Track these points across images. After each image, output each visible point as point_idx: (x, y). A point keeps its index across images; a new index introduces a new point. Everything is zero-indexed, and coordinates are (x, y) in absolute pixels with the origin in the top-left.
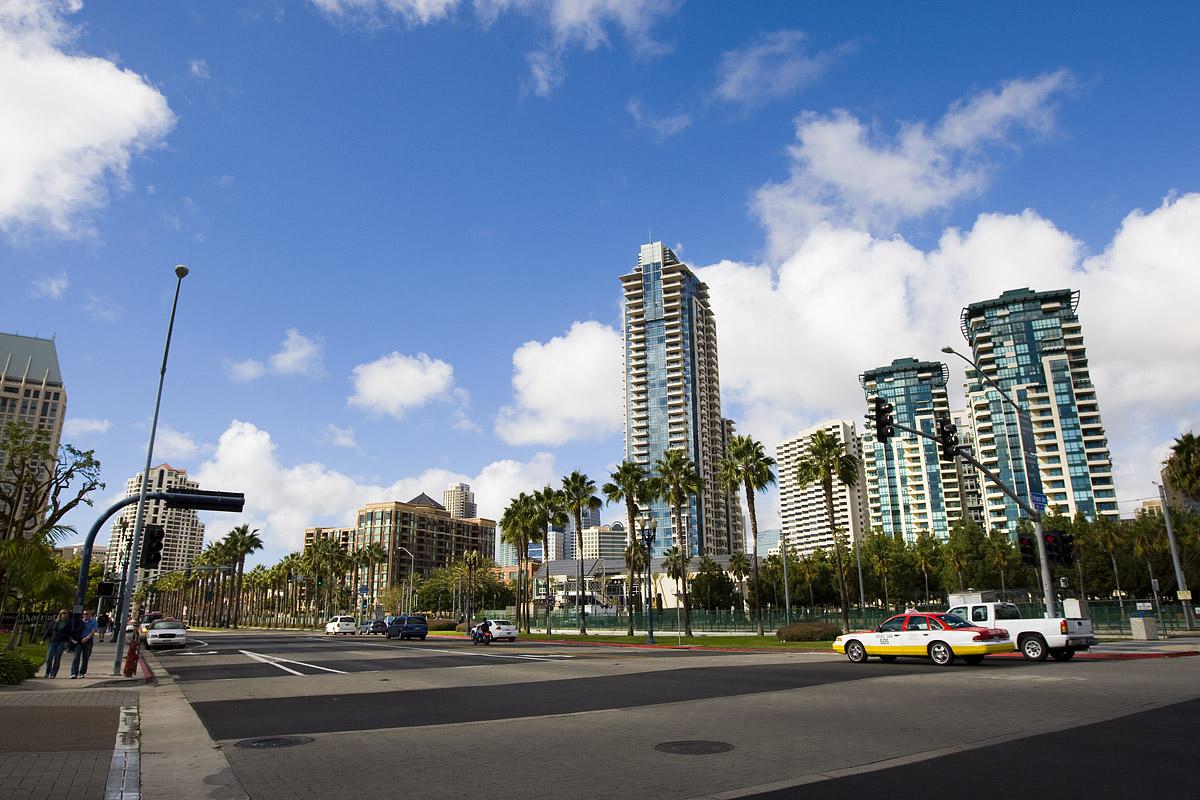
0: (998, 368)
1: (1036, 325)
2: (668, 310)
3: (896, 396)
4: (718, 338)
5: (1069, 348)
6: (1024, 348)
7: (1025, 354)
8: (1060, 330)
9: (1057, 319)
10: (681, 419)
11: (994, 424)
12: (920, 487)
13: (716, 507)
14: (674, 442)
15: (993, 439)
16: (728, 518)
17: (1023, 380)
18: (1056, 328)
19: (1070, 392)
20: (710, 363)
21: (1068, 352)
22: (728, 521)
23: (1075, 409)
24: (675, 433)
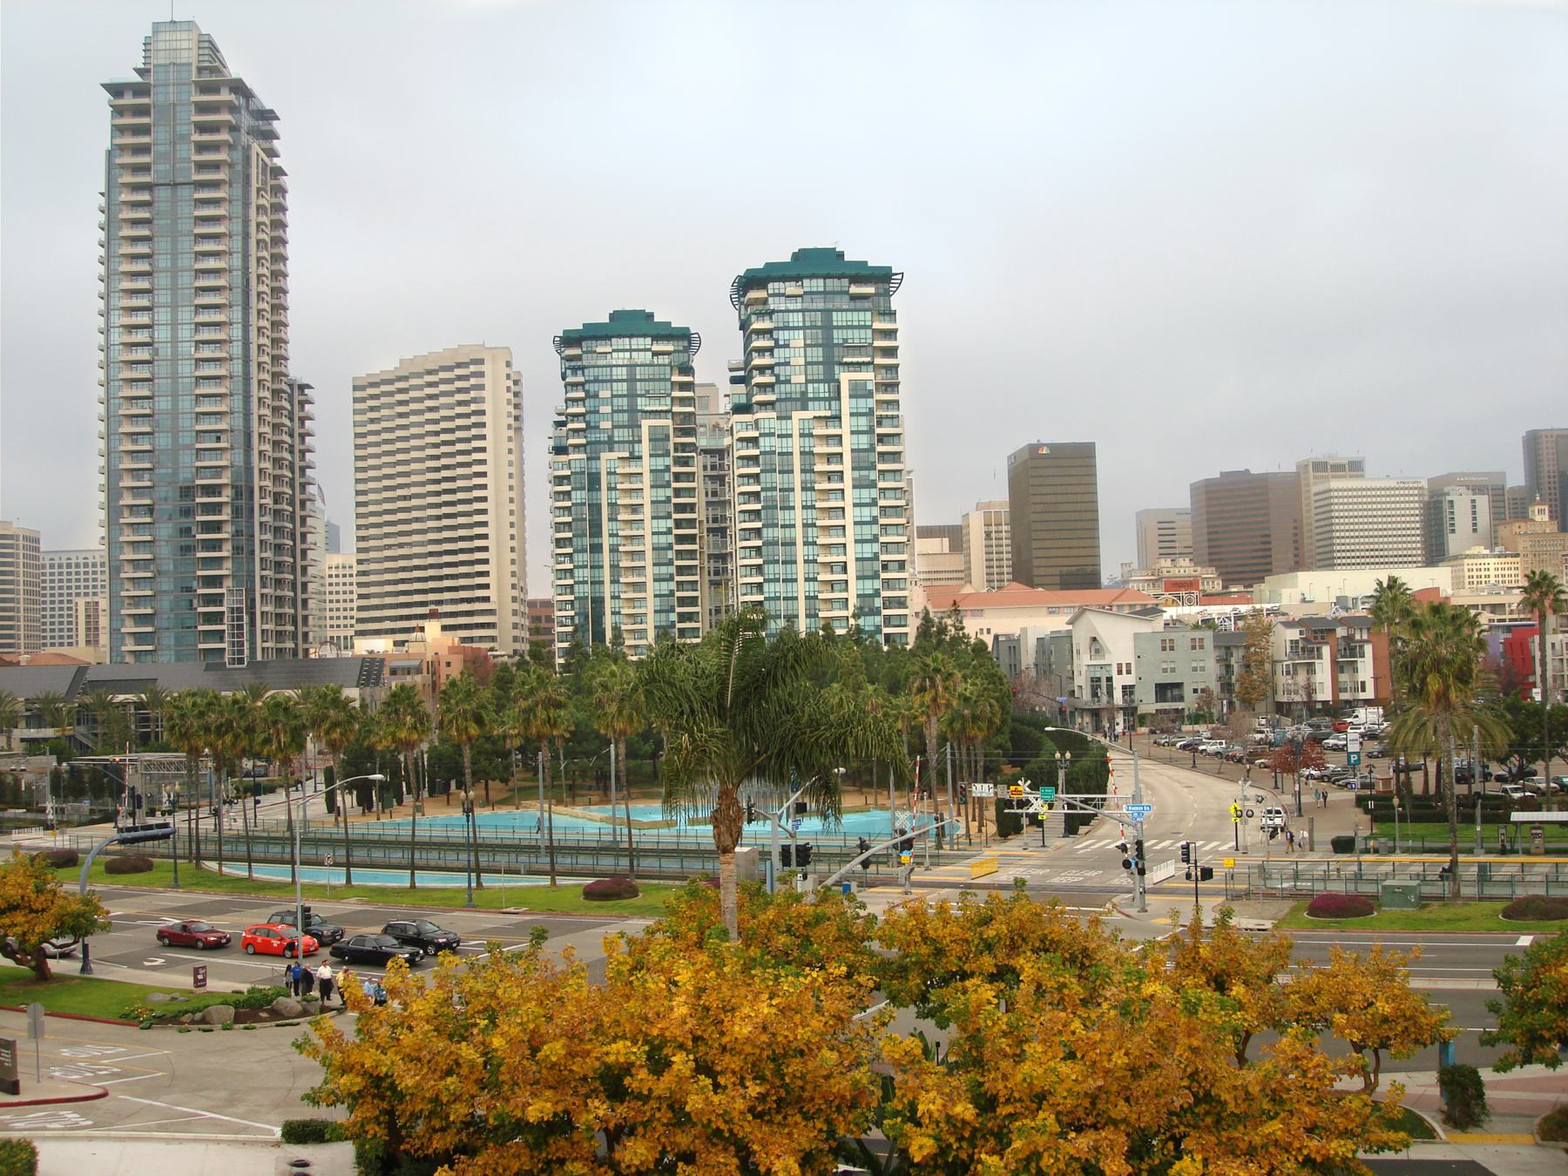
1: (838, 318)
2: (201, 166)
3: (612, 381)
5: (878, 361)
9: (869, 314)
12: (639, 587)
13: (276, 502)
15: (756, 457)
17: (810, 404)
18: (865, 327)
21: (877, 368)
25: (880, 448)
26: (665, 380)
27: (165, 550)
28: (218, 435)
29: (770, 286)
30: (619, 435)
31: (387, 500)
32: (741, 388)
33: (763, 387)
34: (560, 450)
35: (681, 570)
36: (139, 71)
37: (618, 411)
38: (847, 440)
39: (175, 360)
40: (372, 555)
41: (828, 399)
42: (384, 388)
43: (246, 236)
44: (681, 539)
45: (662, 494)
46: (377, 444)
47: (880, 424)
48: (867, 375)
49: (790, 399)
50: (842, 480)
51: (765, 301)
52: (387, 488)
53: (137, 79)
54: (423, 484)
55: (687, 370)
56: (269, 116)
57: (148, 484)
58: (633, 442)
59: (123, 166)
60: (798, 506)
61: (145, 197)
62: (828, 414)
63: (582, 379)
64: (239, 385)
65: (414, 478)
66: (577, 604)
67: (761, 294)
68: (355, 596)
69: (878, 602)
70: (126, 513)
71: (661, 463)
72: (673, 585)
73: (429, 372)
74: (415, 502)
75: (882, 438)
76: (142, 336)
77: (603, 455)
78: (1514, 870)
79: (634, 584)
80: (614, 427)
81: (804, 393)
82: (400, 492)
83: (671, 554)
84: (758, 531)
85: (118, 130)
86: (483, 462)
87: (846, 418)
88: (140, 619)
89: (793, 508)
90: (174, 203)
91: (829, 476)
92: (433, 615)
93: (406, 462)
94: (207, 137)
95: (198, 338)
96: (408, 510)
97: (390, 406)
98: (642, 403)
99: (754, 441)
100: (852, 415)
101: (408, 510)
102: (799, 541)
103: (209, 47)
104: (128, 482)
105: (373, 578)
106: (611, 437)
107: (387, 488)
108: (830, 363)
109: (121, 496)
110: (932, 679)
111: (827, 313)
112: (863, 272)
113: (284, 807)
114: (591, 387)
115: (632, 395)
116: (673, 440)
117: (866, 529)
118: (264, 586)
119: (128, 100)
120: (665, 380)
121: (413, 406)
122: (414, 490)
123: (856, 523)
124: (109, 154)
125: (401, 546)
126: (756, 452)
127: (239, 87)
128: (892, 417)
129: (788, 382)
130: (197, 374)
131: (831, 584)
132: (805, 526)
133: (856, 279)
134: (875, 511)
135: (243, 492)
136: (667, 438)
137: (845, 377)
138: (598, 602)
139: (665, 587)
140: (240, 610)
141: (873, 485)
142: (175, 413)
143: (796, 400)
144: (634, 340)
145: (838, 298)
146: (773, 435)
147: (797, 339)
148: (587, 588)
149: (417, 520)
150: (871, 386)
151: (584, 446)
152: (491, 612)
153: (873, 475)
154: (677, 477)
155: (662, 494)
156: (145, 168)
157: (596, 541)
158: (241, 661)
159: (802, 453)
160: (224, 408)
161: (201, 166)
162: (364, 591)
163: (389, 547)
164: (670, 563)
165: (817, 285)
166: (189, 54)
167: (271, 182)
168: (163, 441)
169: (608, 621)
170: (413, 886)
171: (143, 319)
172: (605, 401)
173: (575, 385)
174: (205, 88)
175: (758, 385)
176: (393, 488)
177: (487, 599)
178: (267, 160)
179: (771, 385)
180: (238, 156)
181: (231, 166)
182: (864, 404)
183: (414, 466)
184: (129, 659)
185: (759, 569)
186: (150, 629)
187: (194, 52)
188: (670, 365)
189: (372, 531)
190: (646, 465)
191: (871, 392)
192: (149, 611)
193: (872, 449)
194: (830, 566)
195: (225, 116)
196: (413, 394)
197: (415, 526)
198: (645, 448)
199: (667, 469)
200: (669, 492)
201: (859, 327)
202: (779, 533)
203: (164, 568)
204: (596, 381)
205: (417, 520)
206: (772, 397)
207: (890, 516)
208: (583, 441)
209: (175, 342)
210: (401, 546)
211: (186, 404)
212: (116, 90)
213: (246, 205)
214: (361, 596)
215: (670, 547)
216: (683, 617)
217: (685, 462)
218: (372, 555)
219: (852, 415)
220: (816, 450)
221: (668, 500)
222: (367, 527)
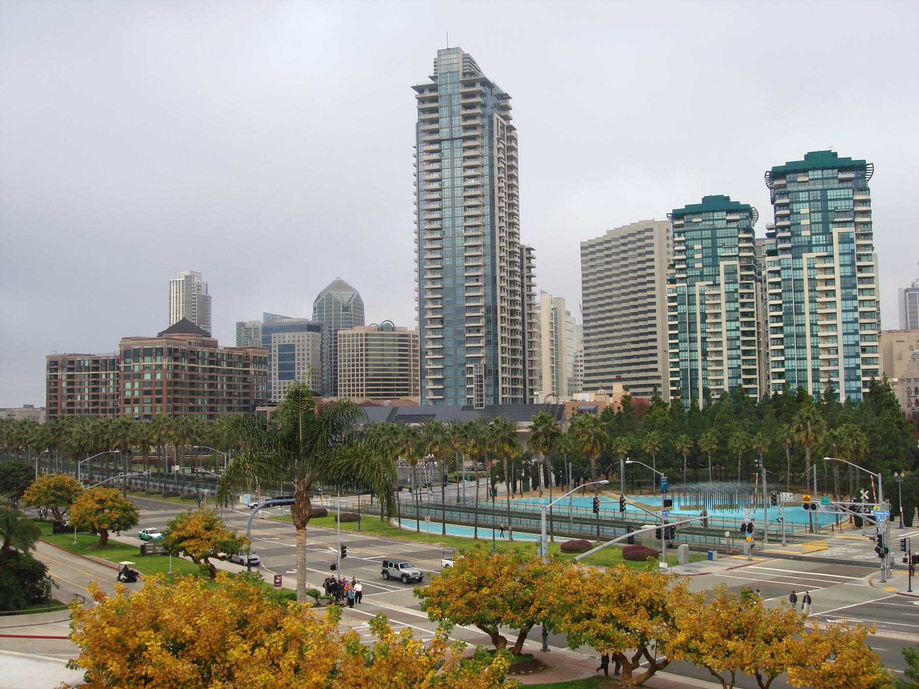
0: (792, 213)
1: (831, 194)
2: (466, 128)
4: (521, 195)
5: (858, 220)
6: (818, 217)
7: (818, 212)
8: (851, 202)
9: (851, 191)
10: (477, 192)
11: (782, 269)
13: (512, 315)
14: (470, 237)
16: (523, 298)
17: (814, 248)
18: (848, 199)
19: (852, 264)
20: (512, 206)
22: (523, 329)
23: (859, 372)
24: (470, 177)
25: (859, 275)
26: (735, 237)
27: (449, 343)
28: (477, 278)
29: (788, 177)
30: (706, 271)
31: (600, 312)
32: (773, 241)
33: (784, 239)
34: (673, 281)
35: (745, 353)
36: (430, 77)
37: (706, 257)
38: (838, 270)
39: (454, 237)
40: (592, 344)
41: (826, 245)
42: (598, 248)
43: (492, 166)
44: (744, 333)
45: (733, 306)
46: (618, 282)
47: (859, 259)
48: (850, 229)
49: (801, 246)
50: (834, 295)
51: (785, 186)
52: (600, 306)
53: (431, 82)
54: (620, 303)
55: (749, 230)
56: (506, 97)
57: (440, 306)
58: (715, 275)
59: (424, 131)
60: (807, 312)
61: (436, 147)
62: (825, 254)
63: (683, 238)
64: (488, 250)
65: (615, 299)
66: (681, 373)
67: (783, 182)
68: (583, 368)
69: (859, 372)
70: (429, 322)
71: (732, 287)
72: (740, 362)
73: (623, 237)
74: (615, 313)
75: (860, 269)
76: (436, 225)
77: (697, 284)
78: (334, 551)
79: (716, 361)
80: (704, 266)
81: (810, 242)
82: (607, 308)
83: (738, 343)
84: (781, 328)
85: (422, 111)
86: (653, 289)
87: (836, 257)
88: (436, 381)
89: (804, 314)
90: (452, 149)
91: (827, 293)
92: (619, 379)
93: (610, 290)
94: (469, 112)
95: (466, 224)
96: (611, 318)
97: (601, 258)
98: (720, 252)
99: (777, 273)
100: (840, 254)
101: (611, 318)
102: (808, 334)
103: (468, 60)
104: (430, 305)
105: (592, 357)
106: (702, 273)
107: (600, 306)
108: (826, 223)
109: (426, 313)
110: (805, 424)
111: (824, 191)
112: (847, 165)
113: (475, 489)
114: (689, 243)
115: (714, 247)
116: (740, 273)
117: (850, 326)
118: (503, 363)
119: (427, 94)
120: (735, 237)
121: (614, 258)
122: (615, 306)
123: (843, 323)
124: (418, 125)
125: (608, 338)
126: (779, 279)
127: (485, 83)
128: (868, 255)
129: (800, 235)
130: (466, 244)
131: (828, 361)
132: (812, 325)
133: (842, 169)
134: (856, 315)
135: (491, 310)
136: (736, 272)
137: (836, 231)
138: (694, 371)
139: (735, 363)
140: (481, 376)
141: (855, 298)
142: (454, 267)
143: (805, 246)
144: (716, 214)
145: (831, 181)
146: (790, 268)
147: (805, 210)
148: (688, 363)
149: (616, 323)
150: (853, 236)
151: (685, 278)
152: (659, 377)
153: (855, 292)
154: (742, 296)
155: (733, 306)
156: (436, 131)
157: (693, 335)
158: (482, 405)
159: (809, 279)
160: (480, 263)
161: (466, 128)
162: (588, 365)
163: (602, 339)
164: (738, 348)
165: (818, 174)
166: (458, 66)
167: (506, 134)
168: (448, 282)
169: (700, 384)
170: (476, 537)
171: (436, 215)
172: (698, 251)
173: (680, 242)
174: (467, 84)
175: (779, 238)
176: (603, 305)
177: (656, 370)
178: (505, 123)
179: (788, 238)
180: (486, 121)
181: (483, 127)
182: (847, 247)
183: (615, 292)
184: (430, 403)
185: (782, 352)
186: (441, 387)
187: (461, 64)
188: (738, 228)
189: (592, 331)
190: (723, 288)
191: (852, 239)
192: (441, 377)
193: (854, 275)
194: (828, 350)
195: (478, 99)
196: (613, 250)
197: (616, 327)
198: (722, 279)
199: (736, 291)
200: (737, 305)
201: (845, 199)
202: (793, 329)
203: (448, 353)
204: (692, 239)
205: (616, 323)
206: (788, 245)
207: (867, 318)
208: (685, 276)
209: (454, 227)
210: (608, 338)
211: (460, 261)
212: (420, 89)
213: (491, 148)
214: (586, 368)
215: (738, 338)
216: (747, 381)
217: (747, 286)
218: (592, 344)
219: (840, 254)
220: (817, 277)
221: (737, 310)
222: (590, 328)
